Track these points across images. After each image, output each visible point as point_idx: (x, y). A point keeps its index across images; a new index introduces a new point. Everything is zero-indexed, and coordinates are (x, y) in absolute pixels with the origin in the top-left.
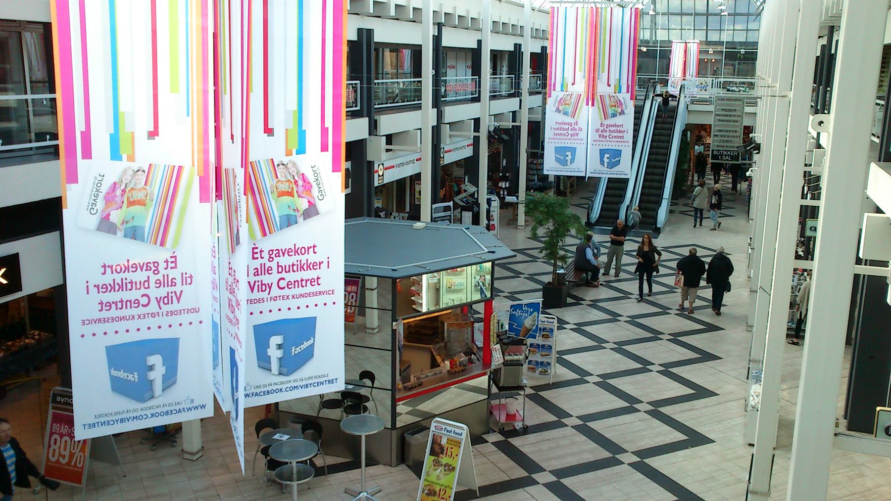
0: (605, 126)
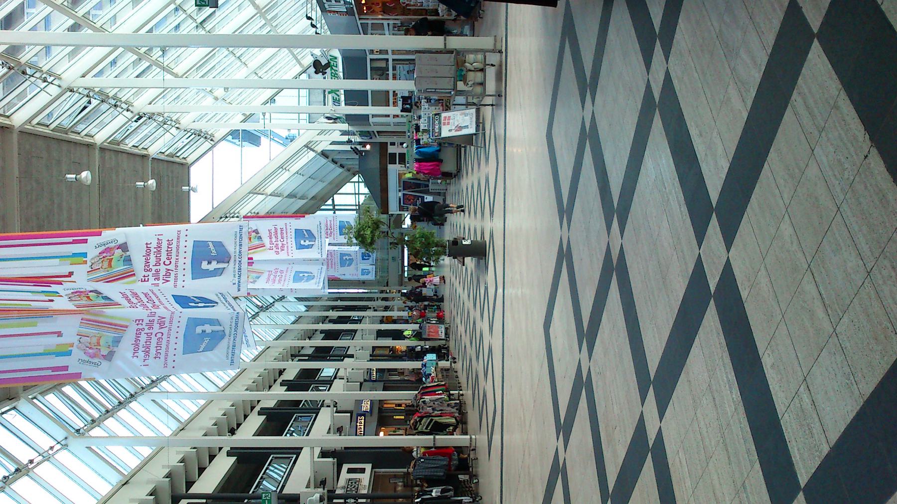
0: (271, 246)
